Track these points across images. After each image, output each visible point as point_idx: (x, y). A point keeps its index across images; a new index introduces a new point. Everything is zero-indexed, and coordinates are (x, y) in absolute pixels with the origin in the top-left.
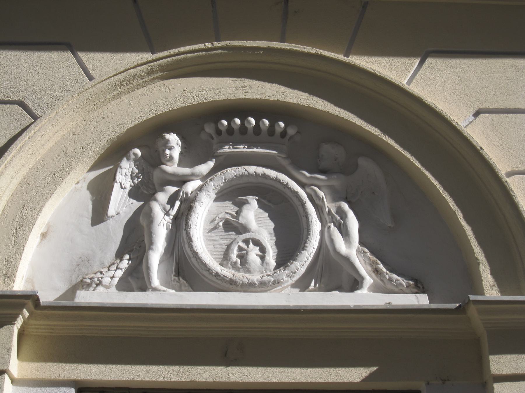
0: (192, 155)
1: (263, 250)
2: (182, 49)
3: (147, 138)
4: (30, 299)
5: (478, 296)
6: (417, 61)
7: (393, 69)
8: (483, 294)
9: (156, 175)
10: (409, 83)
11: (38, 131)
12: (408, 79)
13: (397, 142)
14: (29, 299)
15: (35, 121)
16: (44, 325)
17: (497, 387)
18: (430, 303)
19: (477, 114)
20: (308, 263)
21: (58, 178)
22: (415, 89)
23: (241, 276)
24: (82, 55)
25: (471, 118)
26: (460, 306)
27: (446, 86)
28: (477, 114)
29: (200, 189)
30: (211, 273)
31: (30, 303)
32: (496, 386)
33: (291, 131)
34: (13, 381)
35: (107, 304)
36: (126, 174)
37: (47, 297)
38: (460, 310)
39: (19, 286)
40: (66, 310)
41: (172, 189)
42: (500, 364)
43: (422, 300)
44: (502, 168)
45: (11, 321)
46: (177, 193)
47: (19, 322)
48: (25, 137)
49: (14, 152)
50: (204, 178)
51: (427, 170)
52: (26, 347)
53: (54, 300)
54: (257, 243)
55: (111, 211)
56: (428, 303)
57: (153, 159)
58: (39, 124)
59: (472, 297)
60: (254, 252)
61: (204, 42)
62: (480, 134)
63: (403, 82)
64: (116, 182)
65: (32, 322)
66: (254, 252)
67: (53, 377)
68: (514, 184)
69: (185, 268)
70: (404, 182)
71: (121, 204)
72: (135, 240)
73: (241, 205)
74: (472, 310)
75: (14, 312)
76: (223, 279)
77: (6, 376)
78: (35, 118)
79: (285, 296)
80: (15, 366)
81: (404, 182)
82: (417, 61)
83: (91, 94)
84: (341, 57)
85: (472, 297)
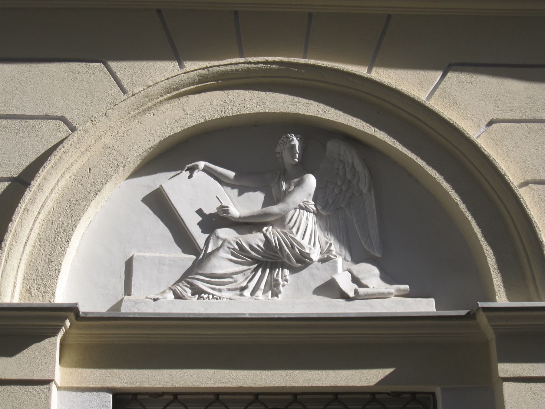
4: (72, 310)
5: (489, 303)
7: (412, 83)
8: (494, 300)
10: (477, 138)
13: (469, 208)
14: (72, 311)
16: (87, 334)
18: (437, 308)
19: (490, 124)
24: (113, 65)
25: (483, 128)
26: (469, 313)
27: (466, 101)
28: (490, 124)
31: (72, 315)
32: (507, 386)
34: (59, 388)
35: (212, 314)
37: (83, 309)
38: (470, 316)
39: (61, 296)
40: (113, 320)
42: (505, 369)
43: (426, 306)
44: (513, 177)
45: (55, 334)
48: (61, 149)
51: (464, 203)
53: (108, 311)
56: (434, 310)
58: (76, 134)
59: (481, 304)
63: (421, 96)
65: (73, 331)
67: (92, 386)
68: (527, 197)
74: (483, 318)
75: (60, 324)
78: (73, 129)
80: (60, 374)
84: (361, 70)
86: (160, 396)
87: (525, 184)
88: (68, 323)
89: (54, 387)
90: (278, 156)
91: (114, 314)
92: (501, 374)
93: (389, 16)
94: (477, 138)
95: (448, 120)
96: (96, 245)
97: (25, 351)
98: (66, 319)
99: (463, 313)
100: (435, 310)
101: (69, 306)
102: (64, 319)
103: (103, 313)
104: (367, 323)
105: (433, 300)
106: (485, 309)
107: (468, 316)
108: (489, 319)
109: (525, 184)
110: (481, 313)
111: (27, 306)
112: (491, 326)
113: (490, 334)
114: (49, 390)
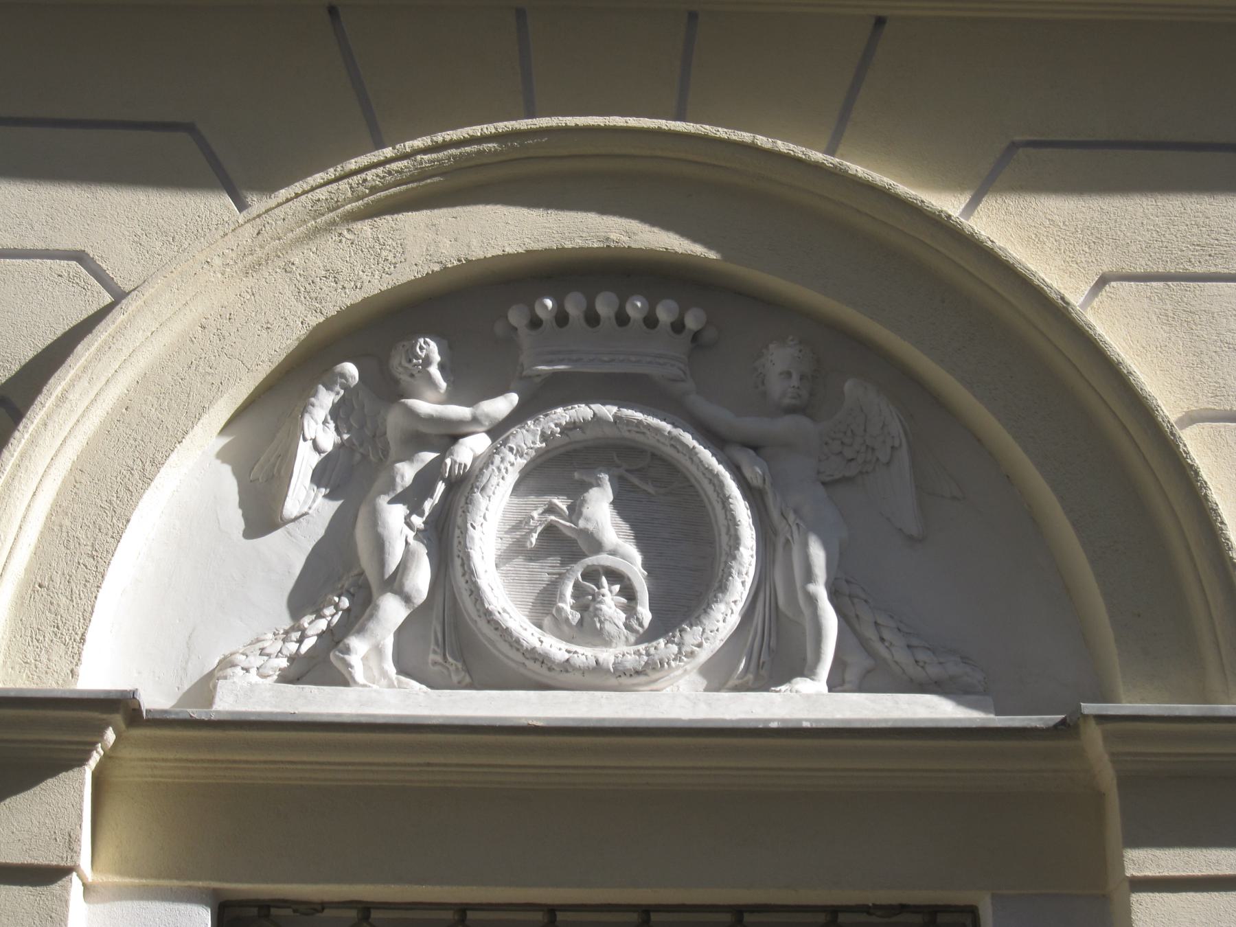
0: (469, 381)
1: (629, 593)
3: (373, 335)
4: (120, 707)
9: (393, 421)
11: (63, 398)
17: (1144, 905)
20: (741, 605)
21: (144, 471)
23: (585, 654)
26: (1063, 722)
28: (1103, 281)
29: (485, 461)
30: (663, 435)
31: (118, 718)
32: (1135, 897)
33: (693, 321)
36: (319, 431)
37: (154, 700)
38: (1068, 729)
39: (96, 675)
41: (428, 456)
42: (1143, 861)
44: (1169, 405)
45: (82, 761)
46: (437, 464)
47: (95, 759)
48: (84, 352)
49: (50, 403)
50: (499, 431)
52: (116, 811)
54: (615, 576)
55: (291, 507)
57: (386, 387)
58: (130, 306)
59: (1089, 708)
60: (610, 602)
62: (1123, 330)
66: (610, 602)
68: (1197, 445)
69: (454, 637)
71: (304, 499)
72: (339, 579)
73: (577, 492)
74: (1094, 736)
75: (89, 739)
76: (542, 659)
77: (74, 874)
78: (119, 296)
79: (681, 695)
83: (201, 284)
85: (1089, 708)
86: (317, 911)
87: (1191, 419)
88: (110, 736)
89: (75, 885)
91: (197, 713)
92: (1131, 871)
93: (880, 21)
97: (327, 525)
98: (106, 727)
102: (100, 731)
103: (165, 712)
104: (451, 738)
106: (1101, 719)
108: (1106, 737)
109: (1191, 419)
110: (1092, 724)
111: (441, 722)
113: (1107, 777)
114: (66, 889)
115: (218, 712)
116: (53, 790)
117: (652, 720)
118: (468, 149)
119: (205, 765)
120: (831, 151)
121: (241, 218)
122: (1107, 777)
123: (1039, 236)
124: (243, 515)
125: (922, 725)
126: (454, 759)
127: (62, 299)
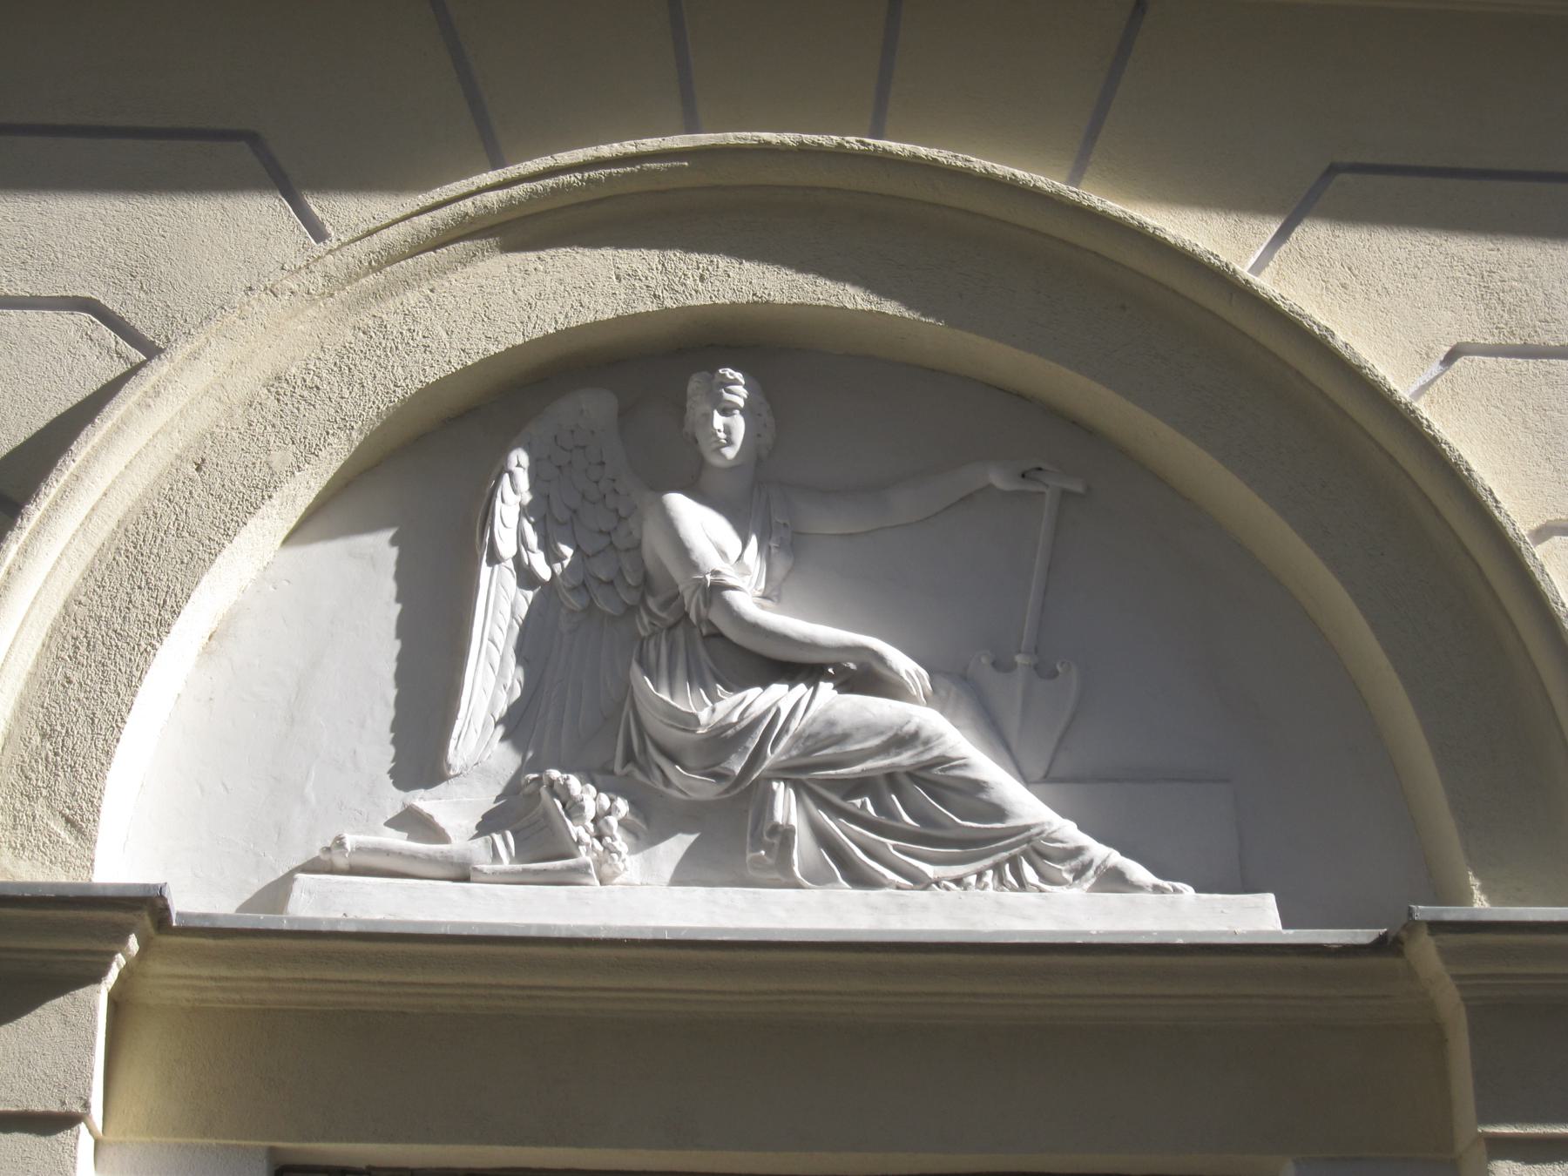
2: (565, 158)
4: (146, 907)
6: (1272, 227)
10: (1257, 269)
12: (1253, 260)
15: (150, 358)
18: (1286, 924)
19: (1450, 358)
22: (1266, 284)
25: (1435, 368)
26: (1382, 940)
28: (1450, 358)
31: (146, 921)
35: (529, 926)
37: (188, 900)
39: (115, 864)
40: (257, 945)
43: (1254, 917)
44: (1518, 512)
45: (97, 978)
58: (159, 370)
59: (1423, 912)
61: (620, 140)
62: (1479, 431)
64: (495, 558)
70: (1184, 540)
74: (1425, 951)
75: (102, 947)
77: (82, 1126)
78: (152, 352)
81: (1184, 540)
82: (1272, 227)
88: (133, 944)
89: (84, 1140)
90: (719, 421)
91: (263, 920)
94: (1257, 269)
95: (1483, 493)
96: (234, 720)
99: (1364, 936)
100: (1279, 927)
101: (141, 894)
102: (122, 940)
103: (225, 916)
105: (1270, 898)
106: (1437, 927)
107: (1380, 946)
108: (1446, 954)
111: (834, 938)
112: (1455, 977)
113: (1450, 1001)
115: (290, 920)
116: (47, 1018)
117: (934, 932)
118: (653, 165)
119: (188, 982)
120: (1074, 180)
121: (320, 248)
122: (1450, 1001)
123: (1379, 300)
124: (401, 658)
125: (109, 893)
126: (565, 981)
127: (76, 357)
